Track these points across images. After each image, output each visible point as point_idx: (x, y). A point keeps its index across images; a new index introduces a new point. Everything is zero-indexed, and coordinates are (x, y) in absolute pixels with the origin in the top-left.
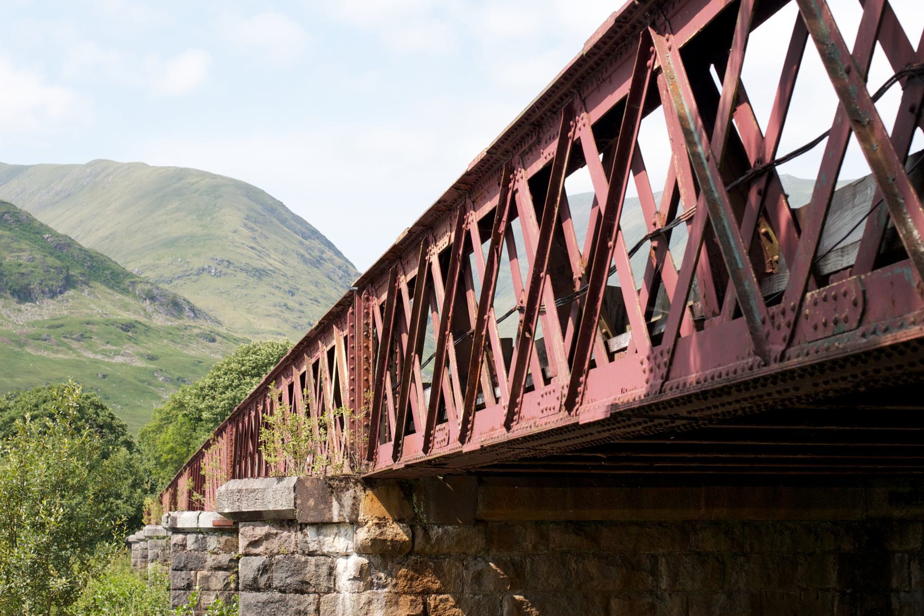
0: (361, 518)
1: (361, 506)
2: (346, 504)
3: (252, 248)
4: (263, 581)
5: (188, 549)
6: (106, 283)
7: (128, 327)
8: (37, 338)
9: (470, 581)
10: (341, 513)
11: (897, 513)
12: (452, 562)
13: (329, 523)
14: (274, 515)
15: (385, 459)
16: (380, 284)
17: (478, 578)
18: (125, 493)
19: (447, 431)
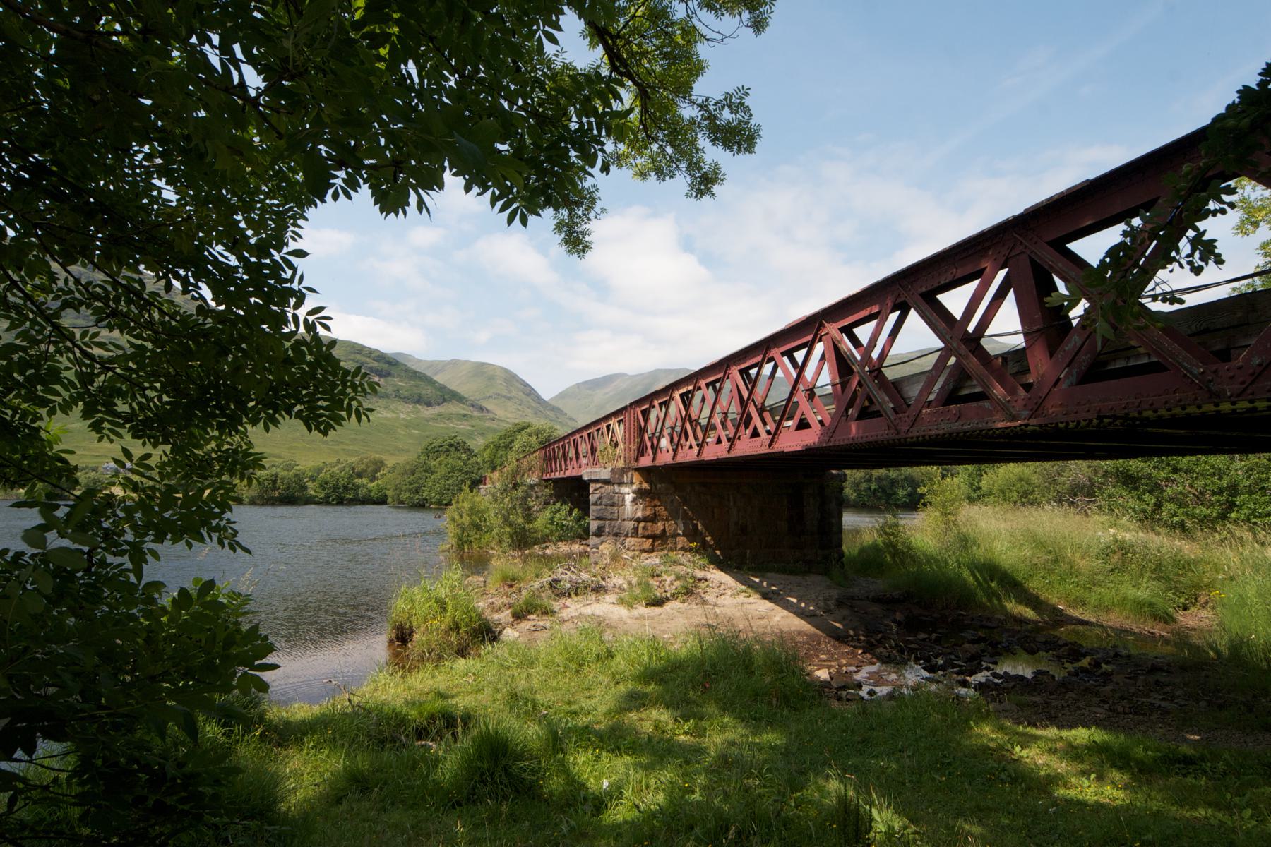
4: (599, 502)
6: (457, 400)
7: (465, 415)
8: (434, 419)
13: (623, 483)
15: (646, 461)
17: (672, 501)
18: (475, 471)
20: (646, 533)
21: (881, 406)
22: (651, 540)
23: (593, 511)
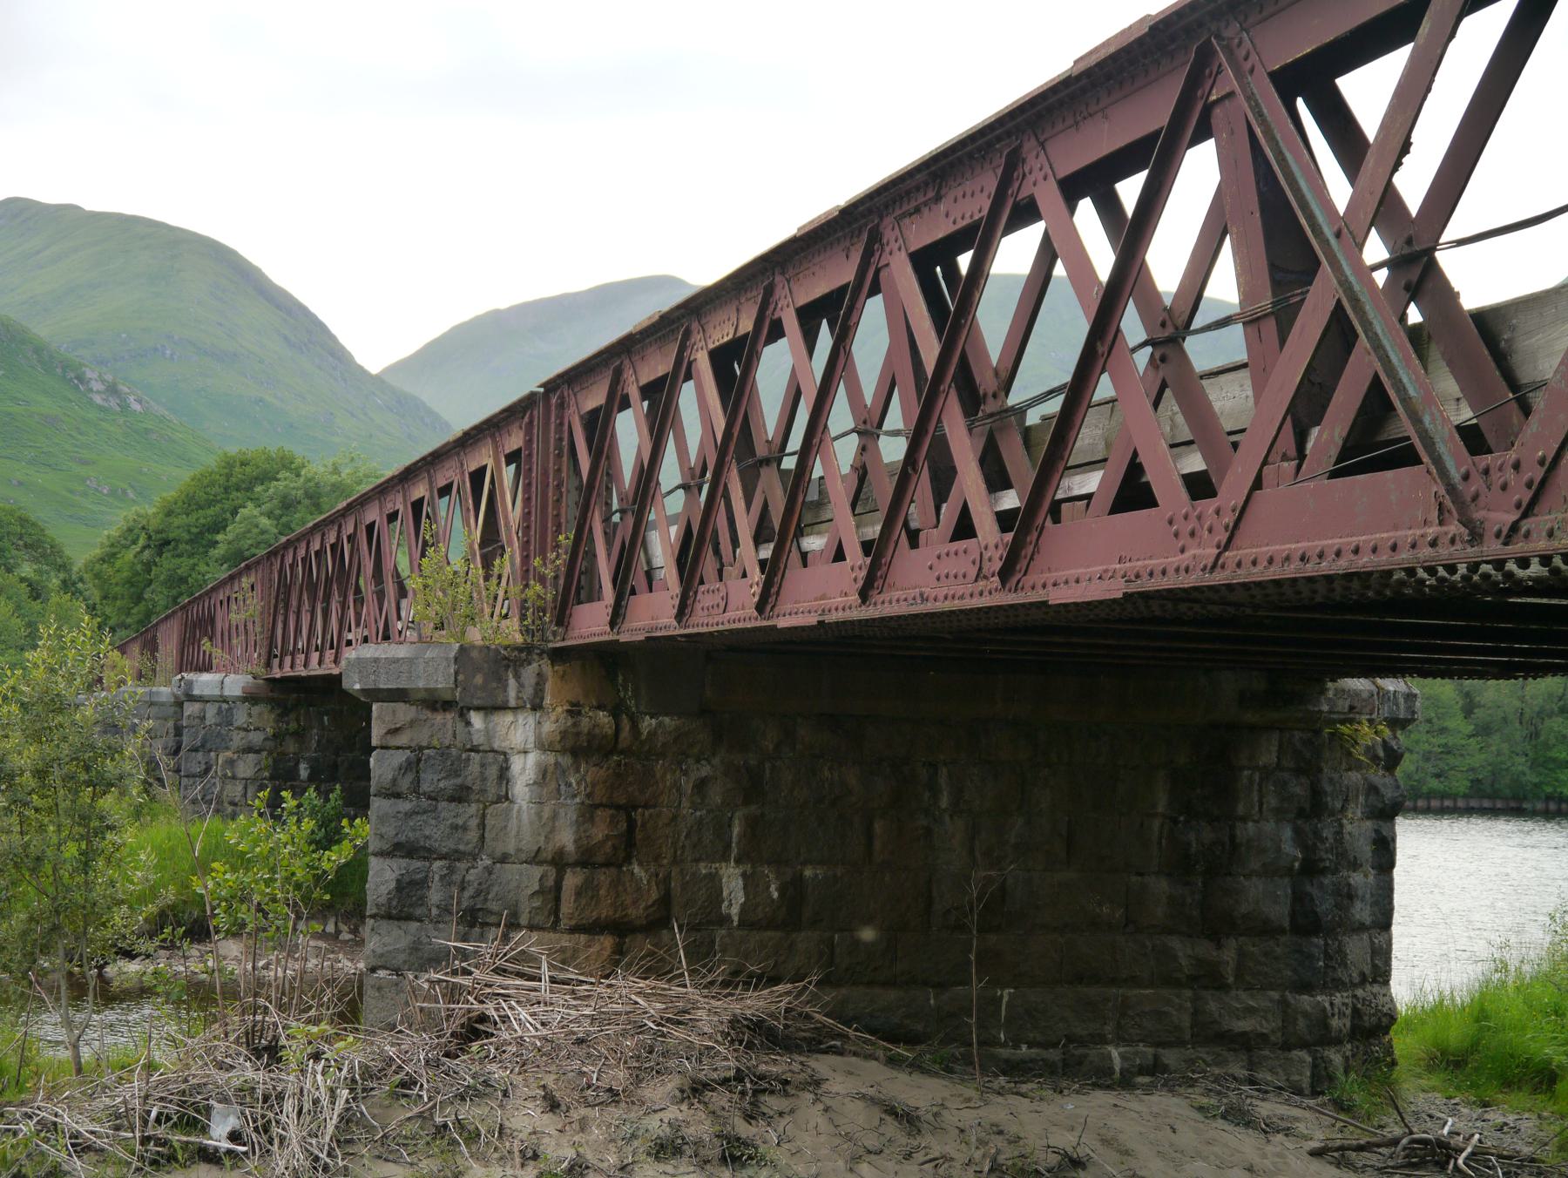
0: (547, 701)
1: (548, 686)
2: (527, 683)
5: (208, 723)
9: (690, 791)
10: (520, 695)
11: (1250, 717)
12: (666, 764)
13: (503, 708)
14: (421, 695)
15: (591, 623)
16: (584, 386)
19: (723, 593)
21: (1416, 420)
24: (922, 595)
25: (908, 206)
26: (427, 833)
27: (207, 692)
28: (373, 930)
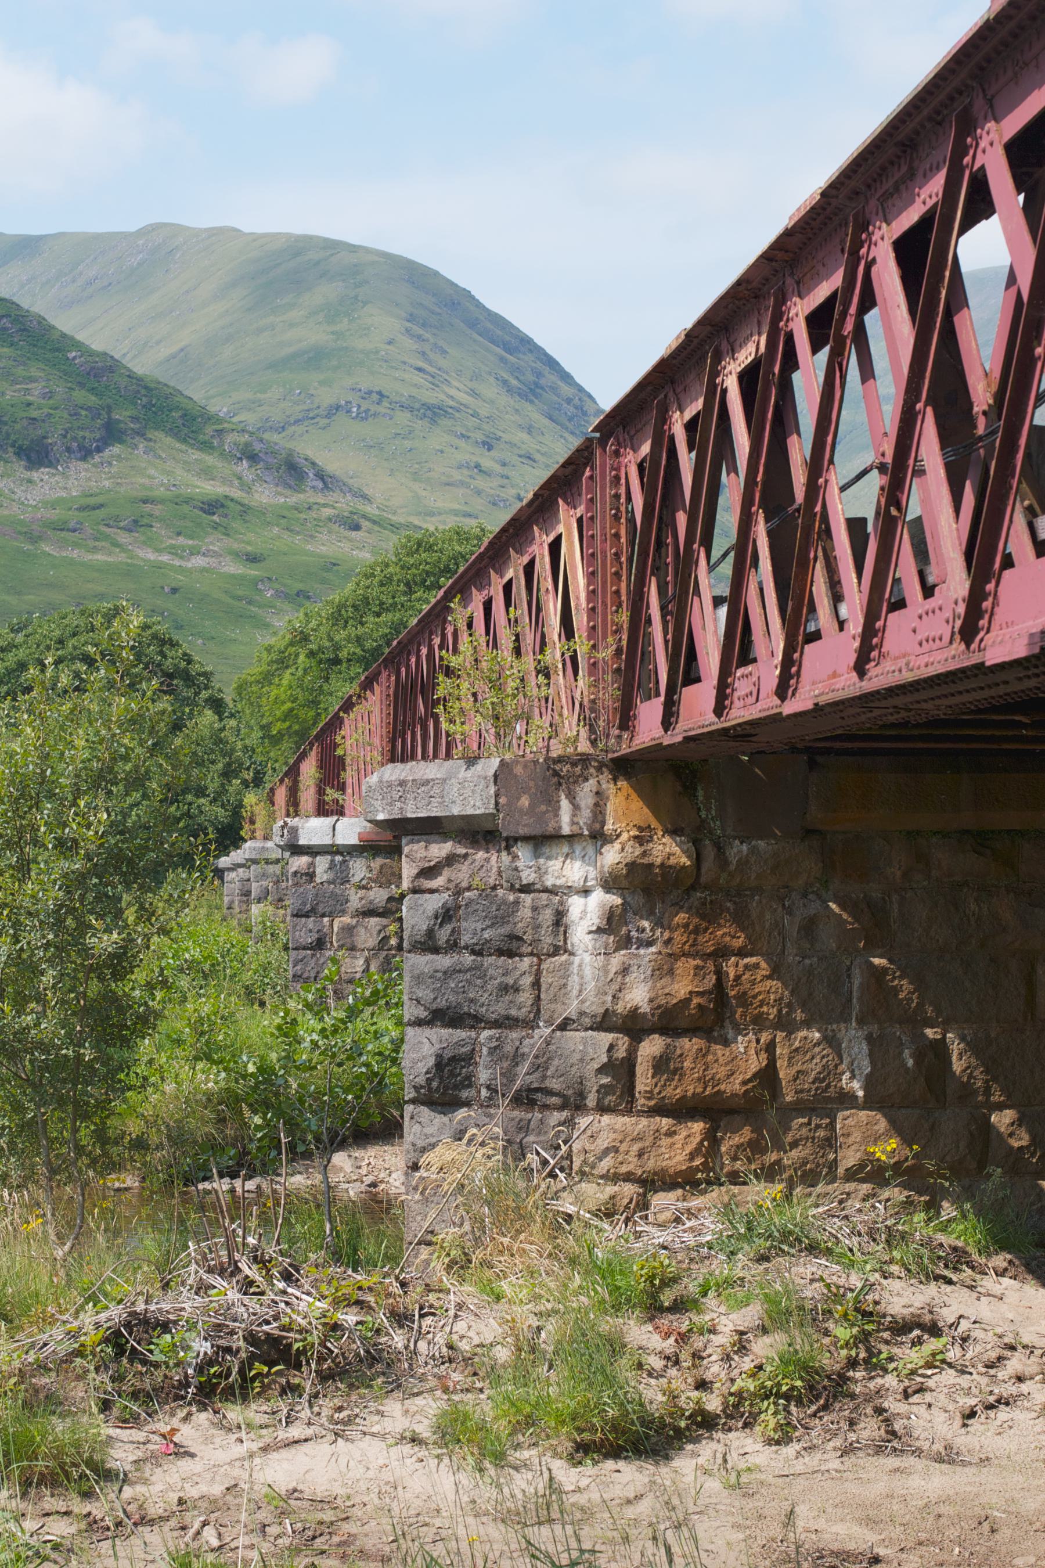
0: (609, 827)
1: (610, 808)
2: (583, 804)
3: (420, 370)
4: (443, 935)
5: (318, 880)
6: (174, 432)
7: (212, 506)
8: (61, 527)
13: (555, 837)
17: (809, 927)
18: (212, 786)
19: (755, 679)
20: (674, 1092)
22: (698, 1127)
23: (418, 979)
24: (907, 664)
25: (888, 185)
26: (471, 995)
27: (316, 841)
28: (412, 1118)
